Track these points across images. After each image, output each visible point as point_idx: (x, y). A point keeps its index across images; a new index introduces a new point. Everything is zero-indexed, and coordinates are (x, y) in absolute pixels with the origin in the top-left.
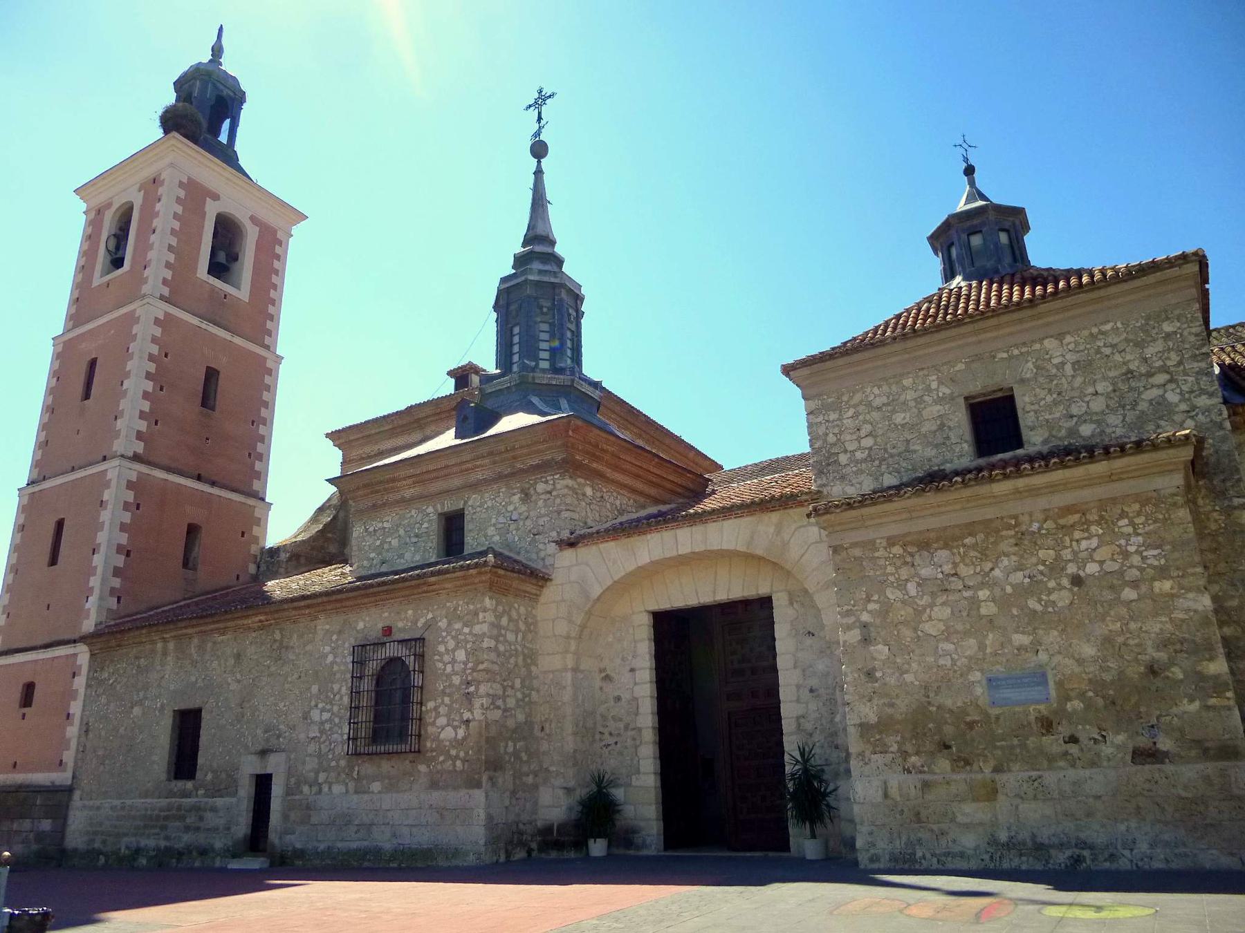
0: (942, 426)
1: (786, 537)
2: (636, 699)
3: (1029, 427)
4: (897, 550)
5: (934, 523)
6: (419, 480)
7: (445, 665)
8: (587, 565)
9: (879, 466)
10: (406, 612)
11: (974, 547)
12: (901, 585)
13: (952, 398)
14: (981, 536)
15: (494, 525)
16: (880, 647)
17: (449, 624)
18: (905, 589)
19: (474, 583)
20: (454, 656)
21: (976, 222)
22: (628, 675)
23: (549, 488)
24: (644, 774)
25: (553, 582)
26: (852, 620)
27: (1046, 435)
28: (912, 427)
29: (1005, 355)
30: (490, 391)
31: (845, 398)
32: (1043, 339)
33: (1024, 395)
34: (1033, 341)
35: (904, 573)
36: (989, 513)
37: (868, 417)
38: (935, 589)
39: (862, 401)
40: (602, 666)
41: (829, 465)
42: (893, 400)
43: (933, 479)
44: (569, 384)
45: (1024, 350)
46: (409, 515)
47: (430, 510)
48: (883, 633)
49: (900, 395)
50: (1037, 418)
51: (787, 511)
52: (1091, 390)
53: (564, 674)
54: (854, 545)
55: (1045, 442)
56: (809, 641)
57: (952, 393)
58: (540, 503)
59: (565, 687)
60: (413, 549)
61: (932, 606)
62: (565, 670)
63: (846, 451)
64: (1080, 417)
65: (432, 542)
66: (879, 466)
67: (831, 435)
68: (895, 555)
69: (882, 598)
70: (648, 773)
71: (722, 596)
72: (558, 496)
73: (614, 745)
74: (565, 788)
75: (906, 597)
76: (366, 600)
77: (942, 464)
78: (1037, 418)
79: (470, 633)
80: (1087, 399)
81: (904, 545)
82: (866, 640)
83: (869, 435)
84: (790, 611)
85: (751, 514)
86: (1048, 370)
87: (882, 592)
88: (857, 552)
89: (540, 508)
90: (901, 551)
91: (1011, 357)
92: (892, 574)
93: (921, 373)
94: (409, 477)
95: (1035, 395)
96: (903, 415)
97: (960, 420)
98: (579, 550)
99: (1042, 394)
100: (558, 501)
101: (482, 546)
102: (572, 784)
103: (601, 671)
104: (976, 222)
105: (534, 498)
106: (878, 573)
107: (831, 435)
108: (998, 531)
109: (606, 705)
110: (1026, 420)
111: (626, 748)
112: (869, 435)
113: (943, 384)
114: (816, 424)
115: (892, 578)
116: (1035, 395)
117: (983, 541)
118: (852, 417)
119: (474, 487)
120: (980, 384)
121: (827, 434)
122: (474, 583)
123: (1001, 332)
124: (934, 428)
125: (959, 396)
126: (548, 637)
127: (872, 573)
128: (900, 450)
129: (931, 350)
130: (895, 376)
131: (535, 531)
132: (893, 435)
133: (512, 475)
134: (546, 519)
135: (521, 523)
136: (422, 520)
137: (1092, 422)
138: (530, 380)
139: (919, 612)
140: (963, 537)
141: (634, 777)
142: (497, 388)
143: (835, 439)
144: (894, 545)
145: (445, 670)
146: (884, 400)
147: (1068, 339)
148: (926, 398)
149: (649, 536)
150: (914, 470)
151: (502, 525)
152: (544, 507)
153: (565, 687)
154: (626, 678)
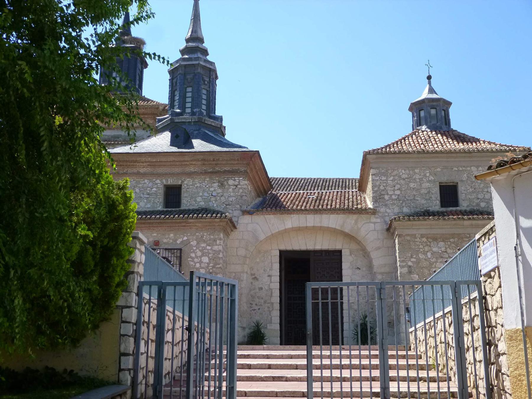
0: (429, 192)
1: (360, 226)
2: (271, 289)
3: (462, 199)
4: (424, 239)
5: (439, 231)
6: (152, 165)
7: (195, 263)
8: (257, 224)
9: (402, 203)
10: (169, 235)
11: (454, 243)
12: (425, 253)
13: (434, 181)
14: (456, 239)
15: (201, 196)
16: (415, 275)
17: (198, 243)
18: (427, 255)
19: (214, 226)
20: (201, 259)
21: (434, 104)
22: (267, 278)
23: (236, 183)
24: (274, 323)
25: (238, 230)
26: (404, 264)
27: (468, 204)
28: (417, 190)
29: (456, 169)
30: (177, 121)
31: (390, 172)
32: (471, 166)
33: (462, 186)
34: (468, 167)
35: (426, 249)
36: (460, 231)
37: (399, 182)
38: (438, 256)
39: (397, 174)
40: (253, 272)
41: (380, 199)
42: (410, 177)
43: (427, 214)
44: (219, 127)
45: (464, 169)
46: (143, 182)
47: (158, 181)
48: (417, 270)
49: (413, 176)
50: (466, 196)
51: (361, 215)
52: (486, 190)
53: (242, 274)
54: (408, 235)
55: (468, 206)
56: (358, 271)
57: (435, 179)
58: (231, 190)
59: (242, 280)
60: (145, 201)
61: (436, 262)
62: (243, 272)
63: (388, 194)
64: (481, 199)
65: (159, 199)
66: (402, 203)
67: (382, 186)
68: (423, 241)
69: (417, 257)
70: (276, 323)
71: (318, 247)
72: (241, 188)
73: (258, 311)
74: (242, 327)
75: (427, 258)
76: (143, 225)
77: (428, 207)
78: (466, 196)
79: (211, 249)
80: (484, 193)
81: (427, 238)
82: (410, 272)
83: (399, 189)
84: (351, 258)
85: (344, 213)
86: (472, 179)
87: (417, 255)
88: (408, 238)
89: (230, 192)
90: (426, 240)
91: (459, 170)
92: (421, 248)
93: (423, 168)
94: (146, 162)
95: (466, 188)
96: (414, 184)
97: (436, 190)
98: (253, 216)
99: (469, 187)
100: (241, 191)
101: (193, 206)
102: (245, 325)
103: (252, 275)
104: (434, 104)
105: (227, 186)
106: (416, 247)
107: (382, 186)
108: (462, 238)
109: (254, 291)
110: (462, 196)
111: (264, 311)
112: (399, 189)
113: (431, 175)
114: (376, 180)
115: (421, 250)
116: (466, 188)
117: (457, 241)
118: (392, 180)
119: (190, 174)
120: (446, 179)
121: (380, 186)
122: (214, 226)
123: (457, 159)
124: (426, 192)
125: (437, 181)
126: (233, 256)
127: (414, 247)
128: (411, 198)
129: (428, 160)
130: (412, 167)
131: (227, 203)
132: (409, 192)
133: (211, 173)
134: (234, 198)
135: (218, 198)
136: (152, 186)
137: (485, 202)
138: (203, 121)
139: (431, 264)
140: (449, 239)
141: (268, 325)
142: (183, 121)
143: (383, 188)
144: (423, 237)
145: (195, 265)
146: (406, 176)
147: (480, 168)
148: (424, 179)
149: (292, 216)
150: (416, 207)
151: (206, 197)
152: (233, 192)
153: (242, 280)
154: (266, 279)
